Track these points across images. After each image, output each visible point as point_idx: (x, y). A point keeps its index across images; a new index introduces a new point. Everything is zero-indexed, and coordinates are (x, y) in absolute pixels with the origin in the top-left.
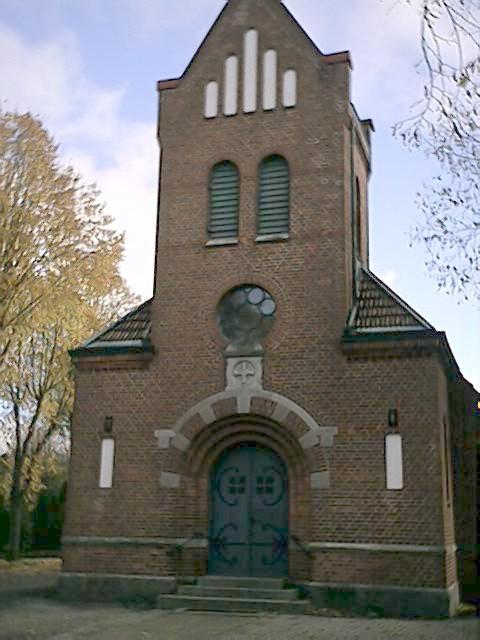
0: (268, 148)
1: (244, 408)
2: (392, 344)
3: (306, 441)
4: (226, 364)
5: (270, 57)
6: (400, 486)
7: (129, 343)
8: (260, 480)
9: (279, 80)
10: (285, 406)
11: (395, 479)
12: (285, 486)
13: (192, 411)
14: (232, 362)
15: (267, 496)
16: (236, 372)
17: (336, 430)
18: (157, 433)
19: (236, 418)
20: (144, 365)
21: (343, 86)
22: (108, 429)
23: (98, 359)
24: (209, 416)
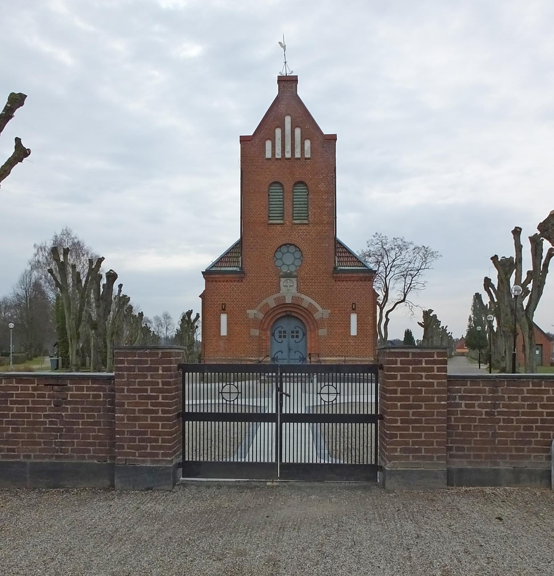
0: (298, 178)
1: (289, 300)
2: (355, 275)
3: (317, 316)
4: (280, 281)
5: (298, 131)
6: (356, 334)
7: (231, 269)
8: (293, 332)
9: (303, 144)
10: (307, 300)
11: (354, 331)
12: (304, 334)
13: (264, 302)
14: (283, 280)
15: (295, 339)
16: (285, 285)
17: (329, 311)
18: (248, 311)
19: (285, 305)
20: (241, 280)
21: (58, 258)
22: (224, 310)
23: (217, 276)
24: (272, 304)
